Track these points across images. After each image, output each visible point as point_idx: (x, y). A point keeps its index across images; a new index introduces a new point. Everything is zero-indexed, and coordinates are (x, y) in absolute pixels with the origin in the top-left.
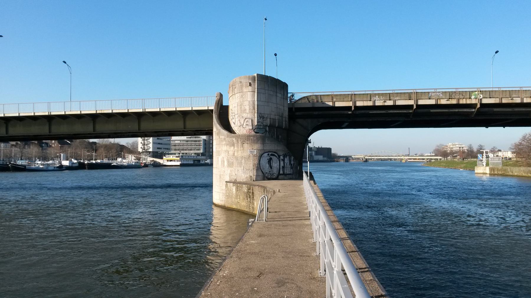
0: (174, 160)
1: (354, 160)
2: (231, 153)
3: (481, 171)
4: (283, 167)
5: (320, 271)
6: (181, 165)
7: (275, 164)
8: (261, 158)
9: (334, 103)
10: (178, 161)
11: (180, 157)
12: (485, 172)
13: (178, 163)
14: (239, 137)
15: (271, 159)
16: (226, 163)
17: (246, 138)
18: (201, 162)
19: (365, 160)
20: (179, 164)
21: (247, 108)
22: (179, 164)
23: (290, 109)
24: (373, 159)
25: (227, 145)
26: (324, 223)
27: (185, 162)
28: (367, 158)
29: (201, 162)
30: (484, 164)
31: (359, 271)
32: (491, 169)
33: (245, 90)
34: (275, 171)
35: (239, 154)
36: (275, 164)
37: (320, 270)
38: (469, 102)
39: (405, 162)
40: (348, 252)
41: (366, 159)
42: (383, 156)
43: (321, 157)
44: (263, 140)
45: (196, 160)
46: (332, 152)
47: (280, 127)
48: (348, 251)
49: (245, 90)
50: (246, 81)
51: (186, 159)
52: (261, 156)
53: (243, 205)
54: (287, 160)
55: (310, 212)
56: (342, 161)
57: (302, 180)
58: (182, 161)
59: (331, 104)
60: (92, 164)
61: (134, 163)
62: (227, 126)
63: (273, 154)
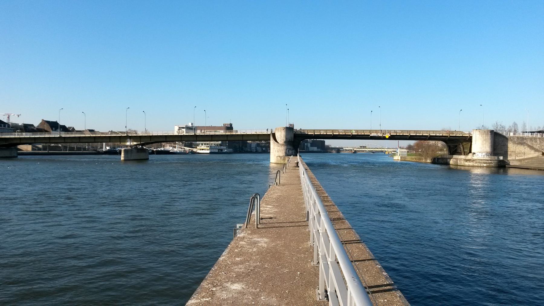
0: (205, 149)
1: (347, 152)
2: (278, 149)
3: (397, 159)
4: (292, 153)
5: (319, 291)
6: (211, 153)
7: (290, 152)
8: (534, 169)
9: (308, 133)
10: (208, 150)
11: (210, 147)
12: (398, 159)
13: (208, 152)
14: (280, 144)
15: (289, 150)
16: (277, 151)
17: (282, 145)
18: (223, 151)
19: (354, 151)
20: (209, 152)
21: (283, 136)
22: (209, 152)
23: (294, 135)
24: (366, 151)
25: (277, 146)
26: (326, 230)
27: (213, 151)
28: (356, 149)
29: (223, 151)
30: (399, 154)
31: (368, 290)
32: (401, 158)
33: (282, 131)
34: (290, 154)
35: (280, 149)
36: (290, 152)
37: (310, 241)
38: (348, 134)
39: (388, 153)
40: (352, 261)
41: (355, 151)
42: (378, 149)
43: (315, 149)
44: (287, 145)
45: (220, 150)
46: (325, 144)
47: (291, 141)
48: (352, 260)
49: (282, 131)
50: (282, 129)
51: (213, 149)
52: (286, 150)
53: (282, 162)
54: (293, 151)
55: (308, 212)
56: (334, 151)
57: (297, 156)
58: (211, 150)
59: (307, 133)
60: (159, 151)
61: (183, 151)
62: (275, 139)
63: (290, 149)
